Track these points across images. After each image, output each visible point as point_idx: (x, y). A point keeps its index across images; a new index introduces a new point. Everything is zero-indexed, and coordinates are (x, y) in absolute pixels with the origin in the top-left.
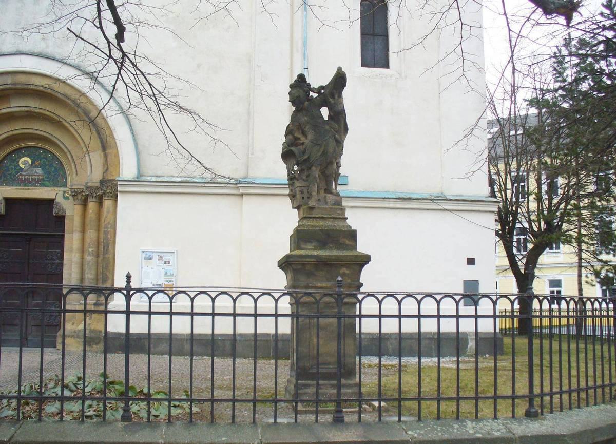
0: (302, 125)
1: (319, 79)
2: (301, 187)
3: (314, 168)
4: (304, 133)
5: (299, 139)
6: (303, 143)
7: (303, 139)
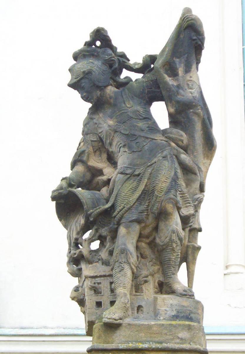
0: (104, 140)
1: (141, 40)
2: (96, 277)
3: (122, 230)
4: (112, 160)
5: (100, 172)
6: (109, 180)
7: (109, 172)
